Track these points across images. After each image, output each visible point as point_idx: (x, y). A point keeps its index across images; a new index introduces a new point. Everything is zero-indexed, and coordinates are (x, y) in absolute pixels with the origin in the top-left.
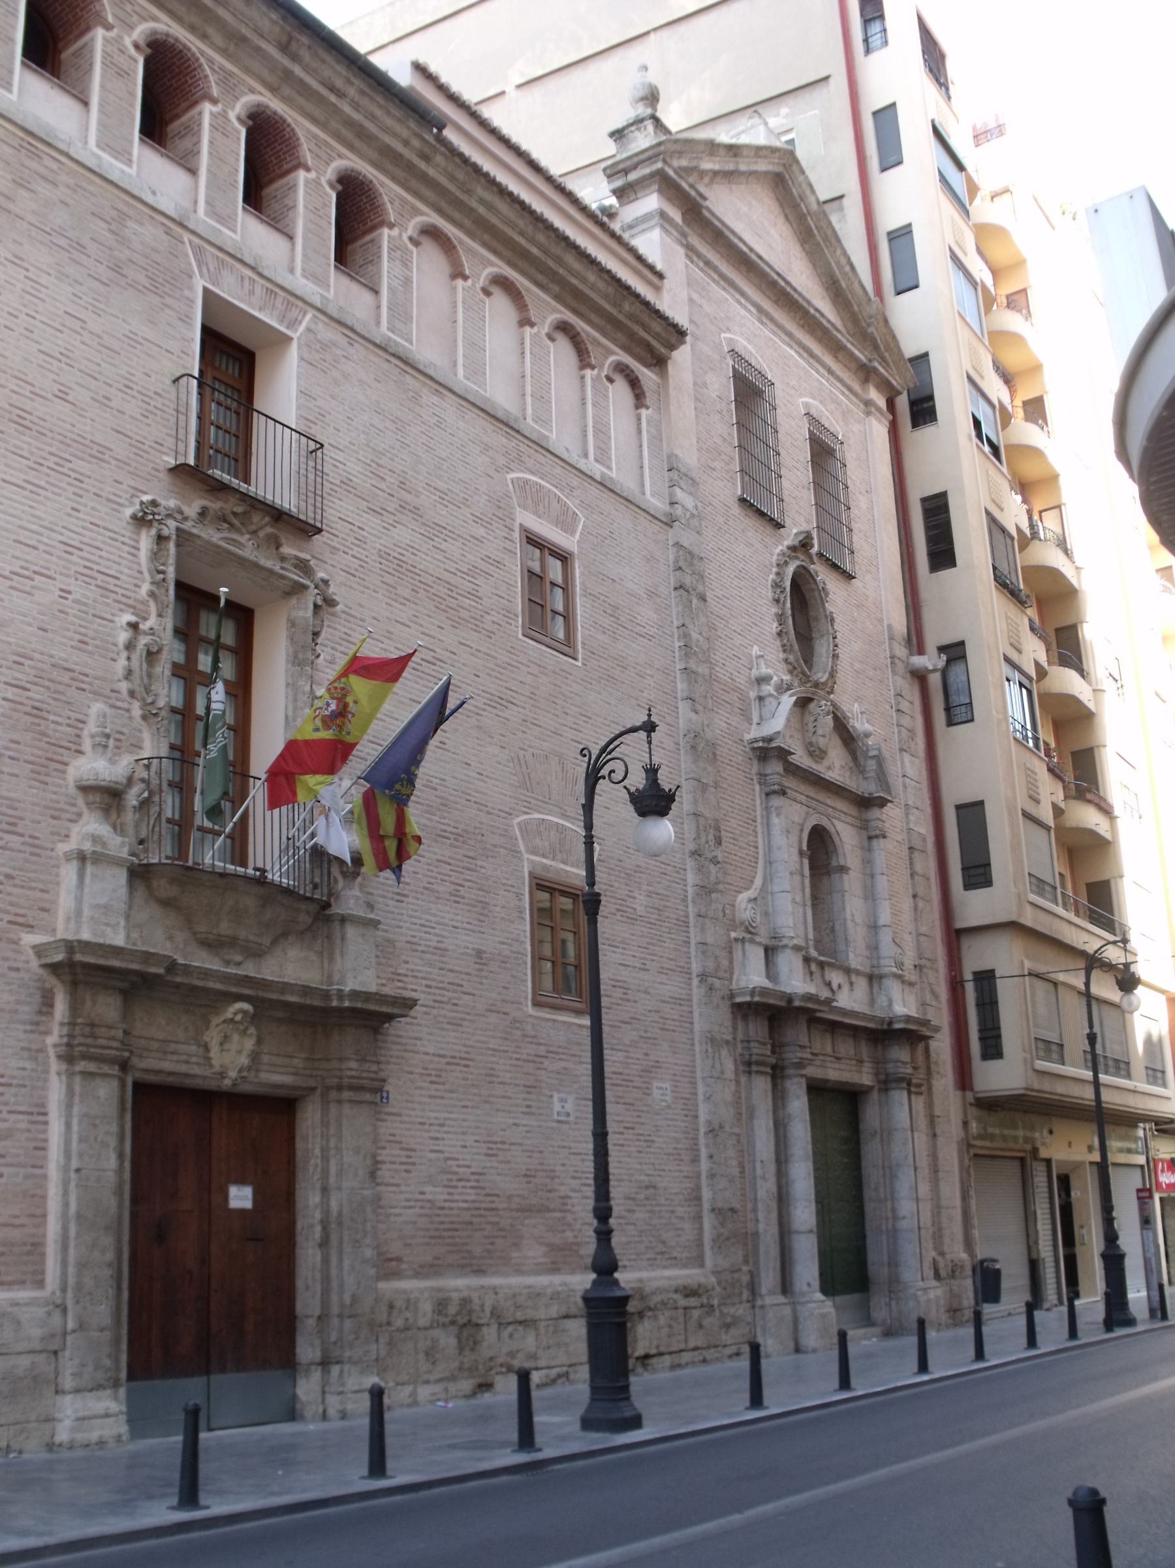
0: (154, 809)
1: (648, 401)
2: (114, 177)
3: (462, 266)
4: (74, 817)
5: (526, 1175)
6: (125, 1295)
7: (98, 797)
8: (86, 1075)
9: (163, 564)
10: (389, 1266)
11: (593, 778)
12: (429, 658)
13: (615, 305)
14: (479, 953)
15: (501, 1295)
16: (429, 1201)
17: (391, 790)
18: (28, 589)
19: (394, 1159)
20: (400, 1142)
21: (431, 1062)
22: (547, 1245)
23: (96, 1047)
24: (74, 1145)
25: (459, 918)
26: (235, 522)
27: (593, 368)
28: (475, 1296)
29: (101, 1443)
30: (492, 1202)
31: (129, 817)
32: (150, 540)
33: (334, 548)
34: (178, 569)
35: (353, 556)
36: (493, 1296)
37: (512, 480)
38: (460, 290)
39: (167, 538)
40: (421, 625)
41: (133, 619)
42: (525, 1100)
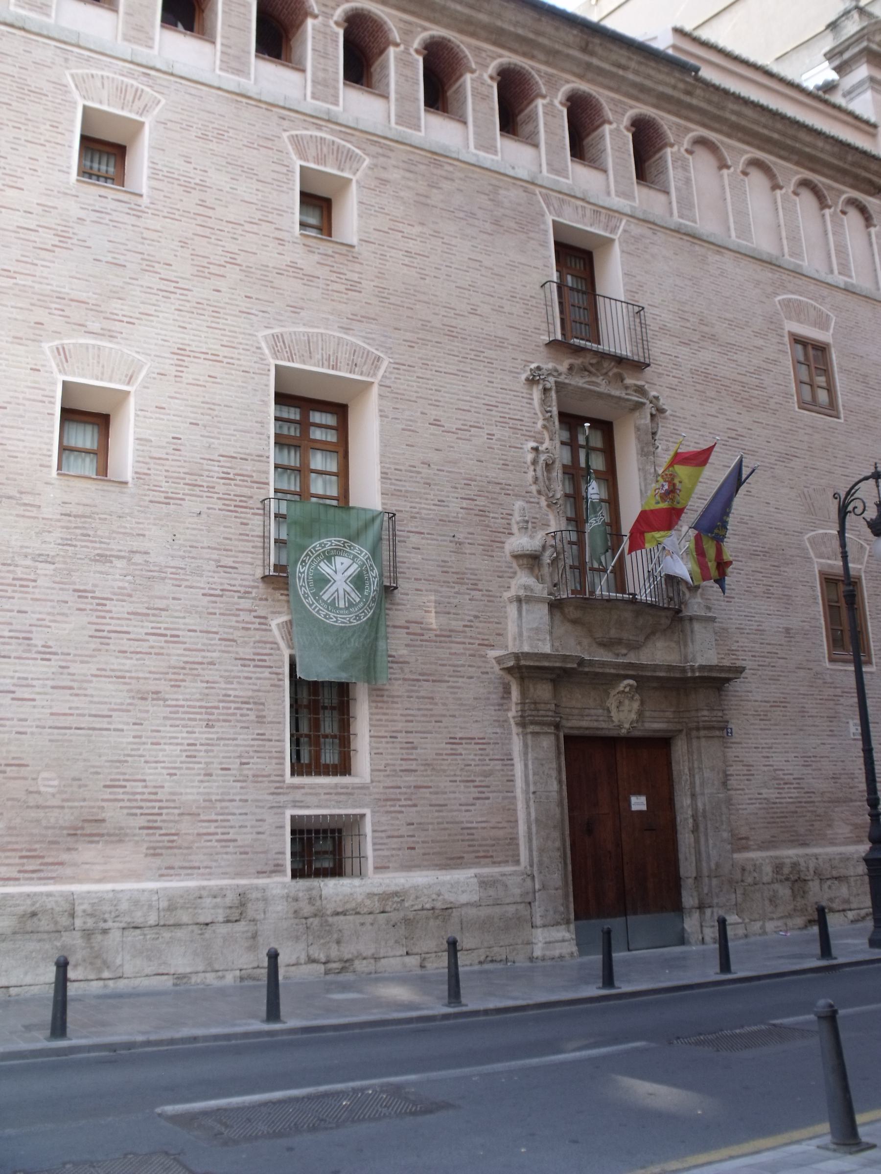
0: (561, 564)
1: (875, 221)
2: (487, 164)
3: (725, 159)
4: (511, 575)
5: (833, 778)
6: (570, 868)
7: (525, 562)
8: (535, 734)
9: (550, 406)
10: (740, 843)
11: (843, 513)
12: (734, 436)
13: (840, 159)
14: (787, 630)
15: (820, 860)
16: (765, 799)
17: (712, 533)
18: (467, 437)
19: (738, 773)
20: (742, 761)
21: (760, 706)
22: (852, 824)
23: (538, 716)
24: (531, 777)
25: (772, 608)
26: (593, 370)
27: (830, 207)
28: (802, 861)
29: (561, 957)
30: (810, 797)
31: (546, 570)
32: (539, 393)
33: (660, 374)
34: (559, 405)
35: (674, 377)
36: (815, 861)
37: (779, 301)
38: (726, 177)
39: (550, 389)
40: (725, 415)
41: (534, 445)
42: (828, 726)
